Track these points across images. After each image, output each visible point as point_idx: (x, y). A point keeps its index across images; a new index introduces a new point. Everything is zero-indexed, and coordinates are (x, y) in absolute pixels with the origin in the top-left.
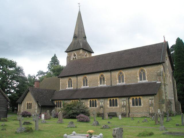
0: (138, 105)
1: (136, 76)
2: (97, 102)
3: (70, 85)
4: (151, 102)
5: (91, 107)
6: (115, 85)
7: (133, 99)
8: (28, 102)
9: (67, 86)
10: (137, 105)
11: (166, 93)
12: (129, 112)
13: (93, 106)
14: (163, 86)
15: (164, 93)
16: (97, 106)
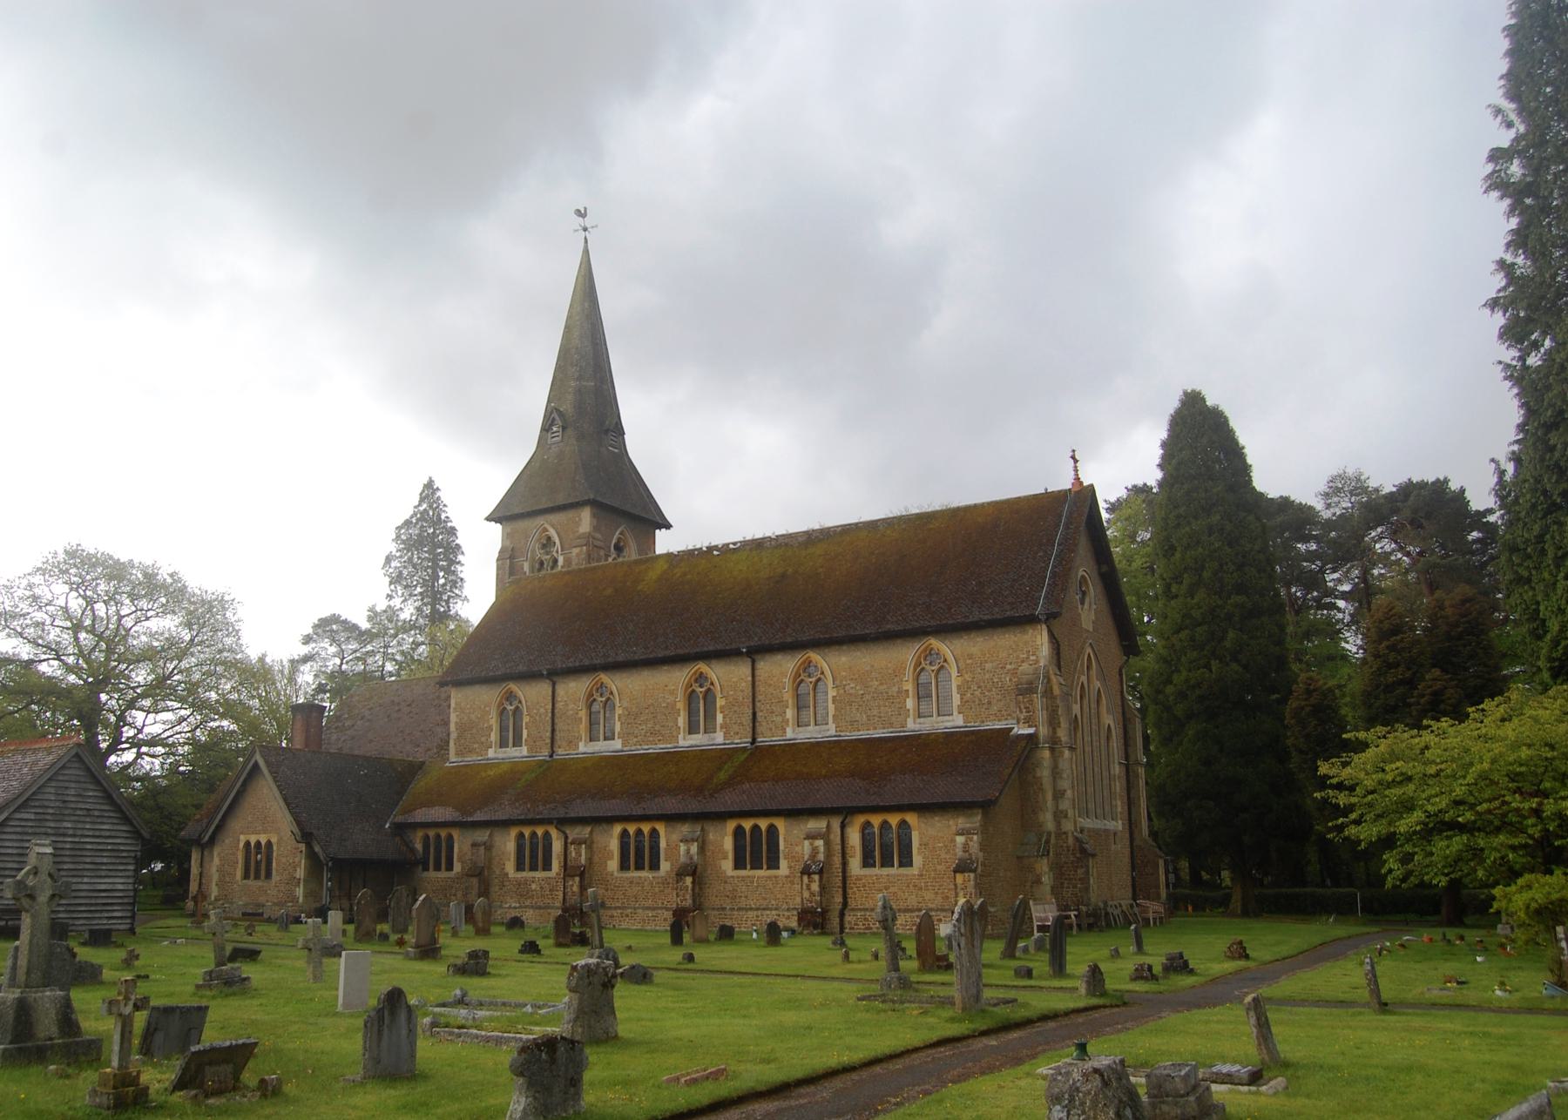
1: (895, 689)
2: (663, 844)
3: (510, 734)
4: (966, 848)
8: (253, 839)
9: (494, 737)
10: (887, 862)
11: (1058, 795)
12: (845, 904)
13: (639, 867)
14: (1047, 754)
15: (1049, 796)
16: (665, 866)
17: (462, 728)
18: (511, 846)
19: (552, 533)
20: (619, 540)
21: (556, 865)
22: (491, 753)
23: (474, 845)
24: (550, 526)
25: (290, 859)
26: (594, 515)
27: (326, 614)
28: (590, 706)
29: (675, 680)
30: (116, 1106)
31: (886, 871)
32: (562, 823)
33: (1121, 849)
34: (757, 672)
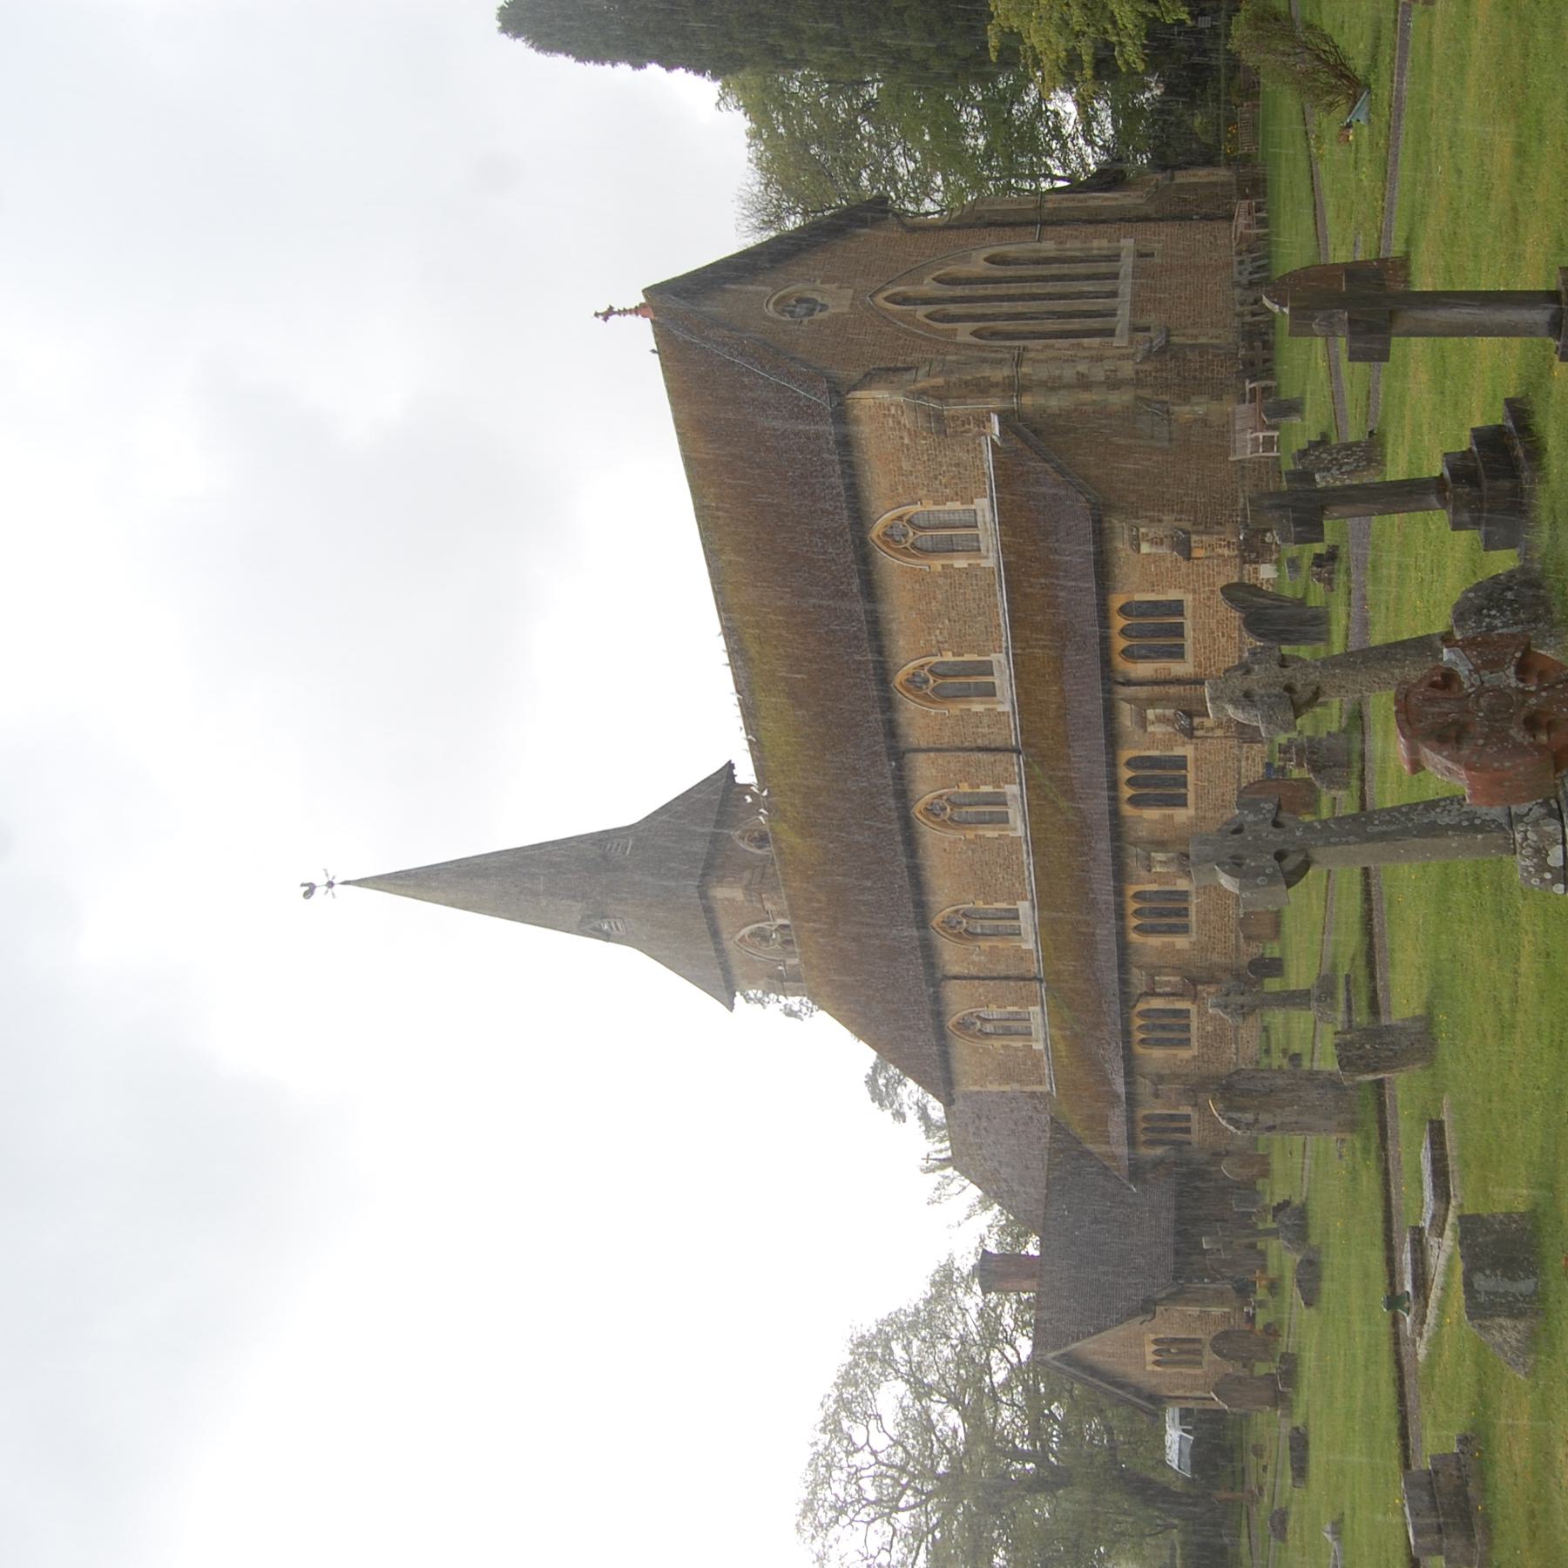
0: (1183, 791)
1: (941, 581)
4: (1152, 542)
5: (1186, 909)
6: (1014, 722)
7: (1128, 654)
11: (1084, 383)
14: (1027, 400)
15: (1085, 396)
17: (1007, 1077)
18: (1158, 1053)
19: (746, 931)
20: (752, 840)
21: (1181, 1005)
22: (1038, 1046)
23: (1157, 1096)
24: (736, 935)
25: (1176, 1321)
26: (720, 880)
27: (866, 1094)
28: (974, 936)
29: (935, 840)
30: (1468, 1529)
31: (1189, 632)
32: (1127, 1000)
33: (1161, 238)
34: (923, 745)
